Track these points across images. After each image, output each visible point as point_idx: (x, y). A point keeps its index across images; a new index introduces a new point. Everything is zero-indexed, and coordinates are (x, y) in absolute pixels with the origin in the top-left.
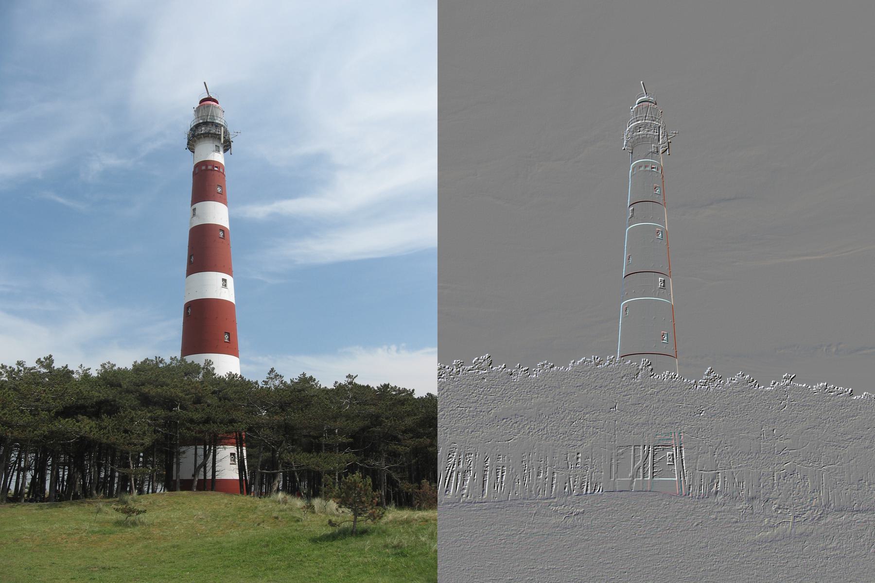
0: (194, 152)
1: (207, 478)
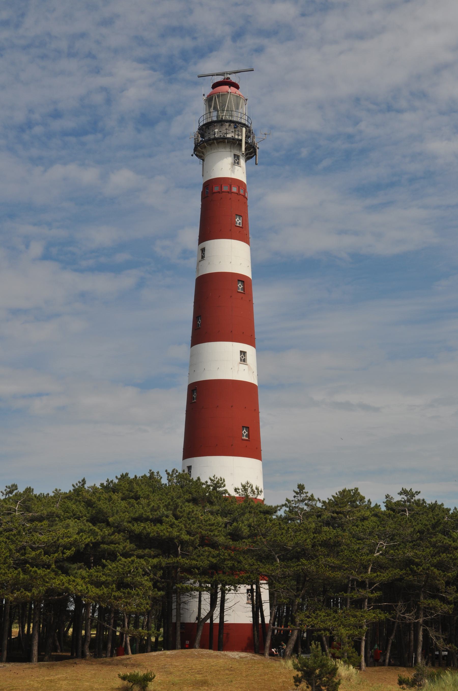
0: (203, 160)
1: (214, 622)
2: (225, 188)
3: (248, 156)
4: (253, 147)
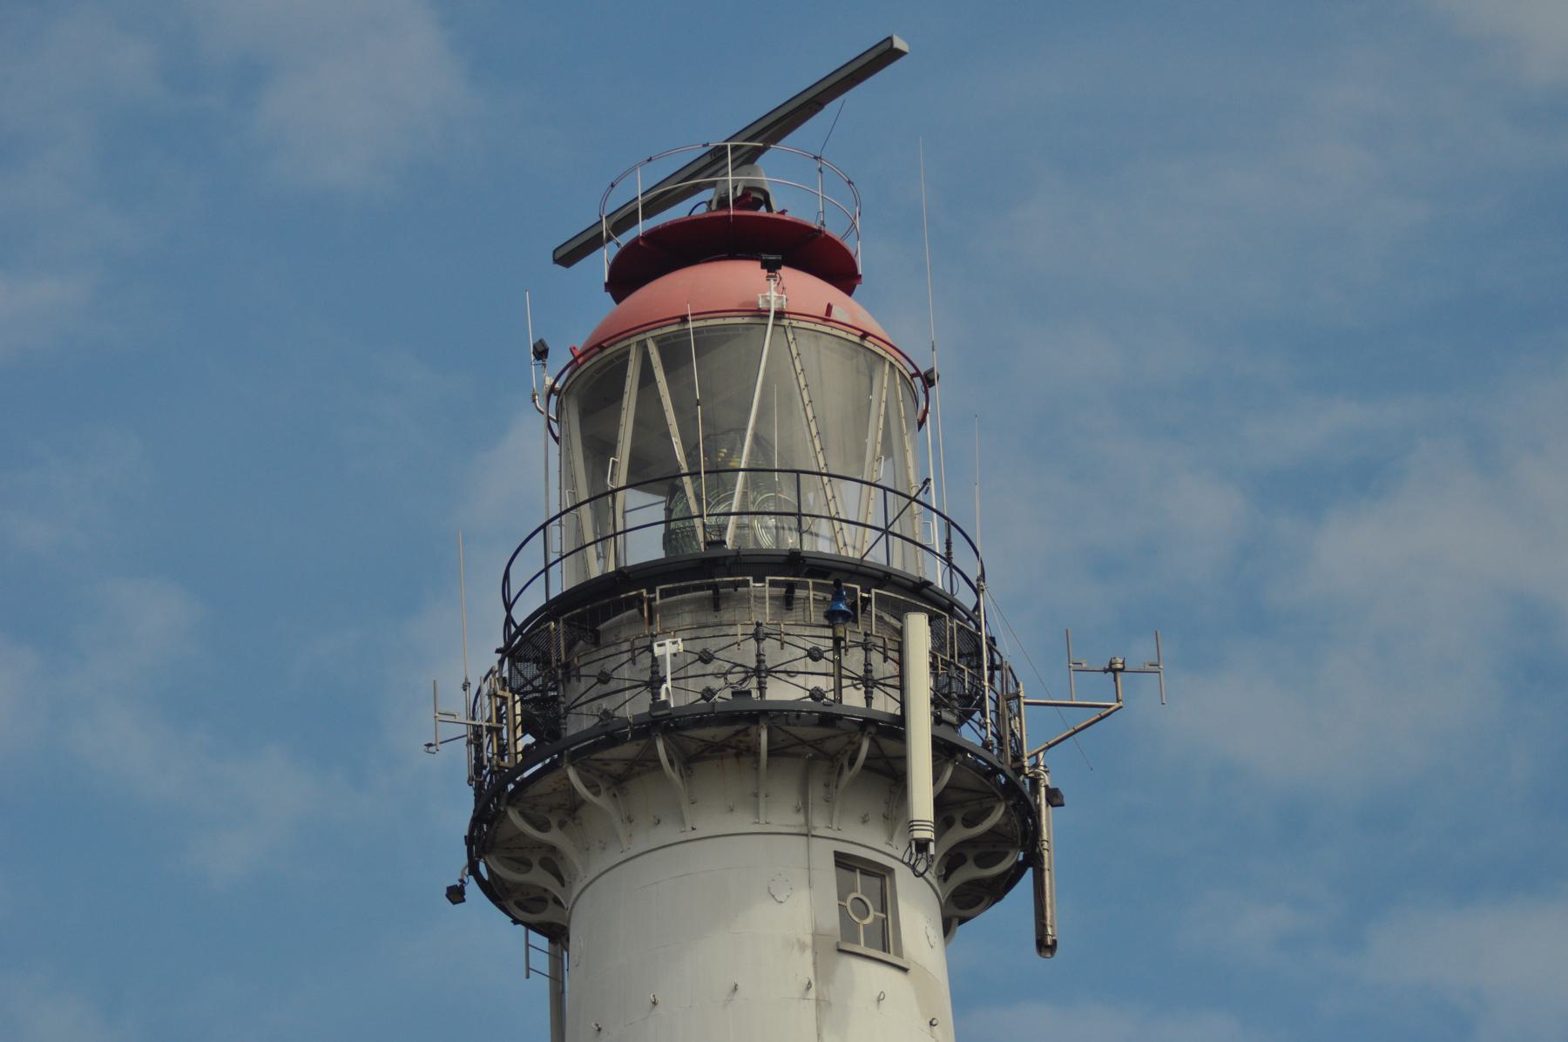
0: (557, 935)
3: (969, 872)
4: (1011, 789)
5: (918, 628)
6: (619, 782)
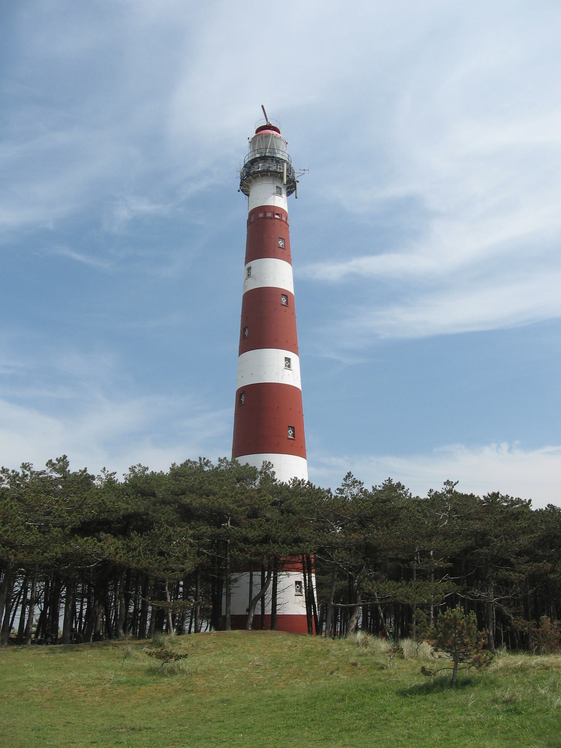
0: (248, 195)
2: (269, 215)
3: (289, 190)
4: (294, 181)
5: (285, 164)
6: (255, 178)
